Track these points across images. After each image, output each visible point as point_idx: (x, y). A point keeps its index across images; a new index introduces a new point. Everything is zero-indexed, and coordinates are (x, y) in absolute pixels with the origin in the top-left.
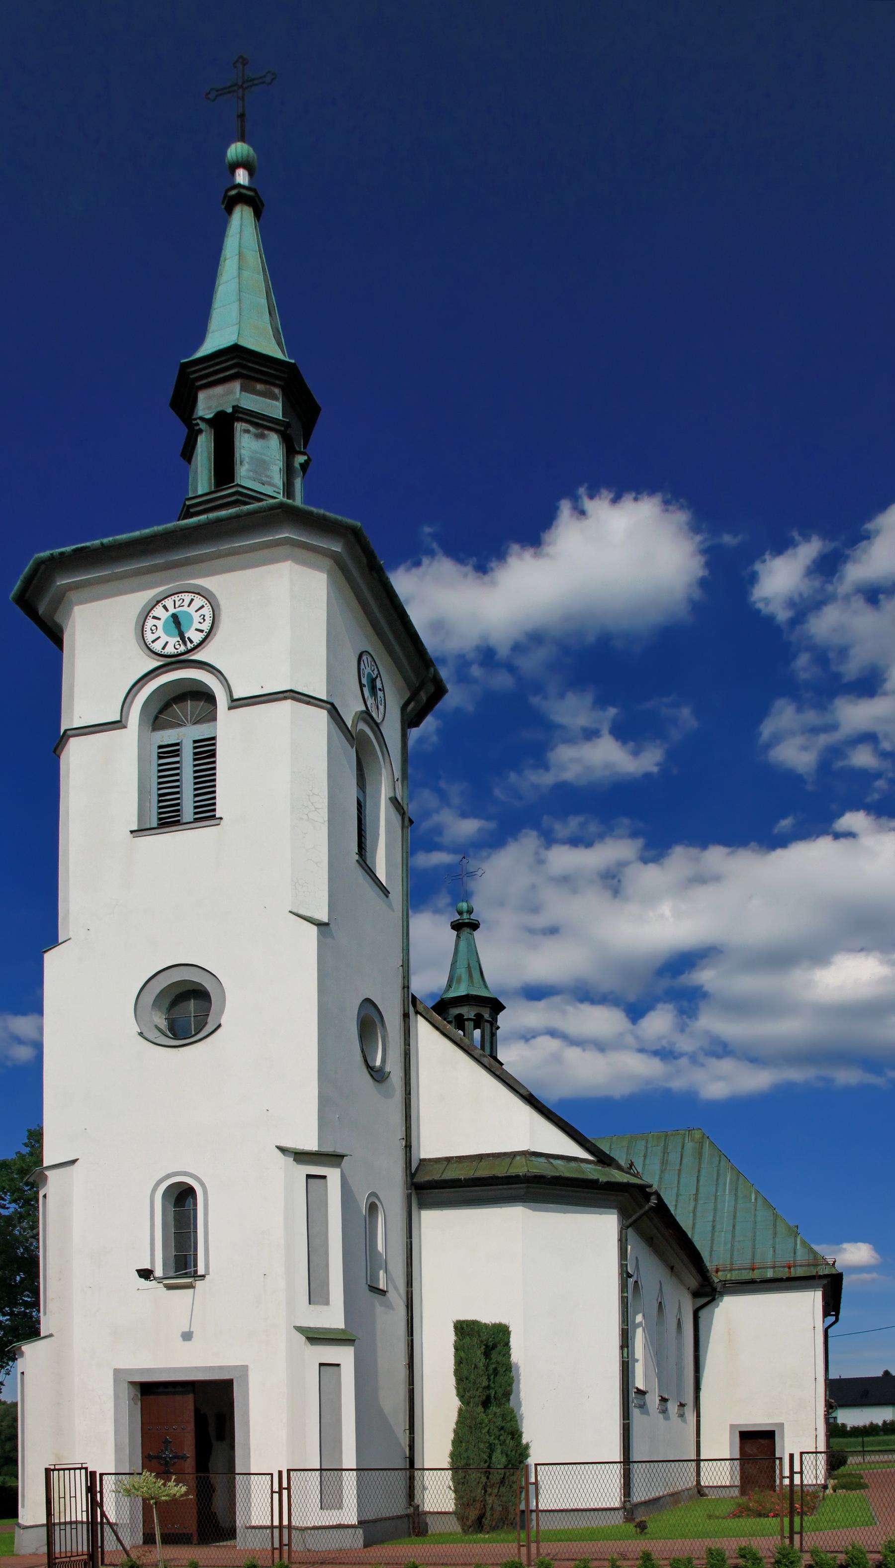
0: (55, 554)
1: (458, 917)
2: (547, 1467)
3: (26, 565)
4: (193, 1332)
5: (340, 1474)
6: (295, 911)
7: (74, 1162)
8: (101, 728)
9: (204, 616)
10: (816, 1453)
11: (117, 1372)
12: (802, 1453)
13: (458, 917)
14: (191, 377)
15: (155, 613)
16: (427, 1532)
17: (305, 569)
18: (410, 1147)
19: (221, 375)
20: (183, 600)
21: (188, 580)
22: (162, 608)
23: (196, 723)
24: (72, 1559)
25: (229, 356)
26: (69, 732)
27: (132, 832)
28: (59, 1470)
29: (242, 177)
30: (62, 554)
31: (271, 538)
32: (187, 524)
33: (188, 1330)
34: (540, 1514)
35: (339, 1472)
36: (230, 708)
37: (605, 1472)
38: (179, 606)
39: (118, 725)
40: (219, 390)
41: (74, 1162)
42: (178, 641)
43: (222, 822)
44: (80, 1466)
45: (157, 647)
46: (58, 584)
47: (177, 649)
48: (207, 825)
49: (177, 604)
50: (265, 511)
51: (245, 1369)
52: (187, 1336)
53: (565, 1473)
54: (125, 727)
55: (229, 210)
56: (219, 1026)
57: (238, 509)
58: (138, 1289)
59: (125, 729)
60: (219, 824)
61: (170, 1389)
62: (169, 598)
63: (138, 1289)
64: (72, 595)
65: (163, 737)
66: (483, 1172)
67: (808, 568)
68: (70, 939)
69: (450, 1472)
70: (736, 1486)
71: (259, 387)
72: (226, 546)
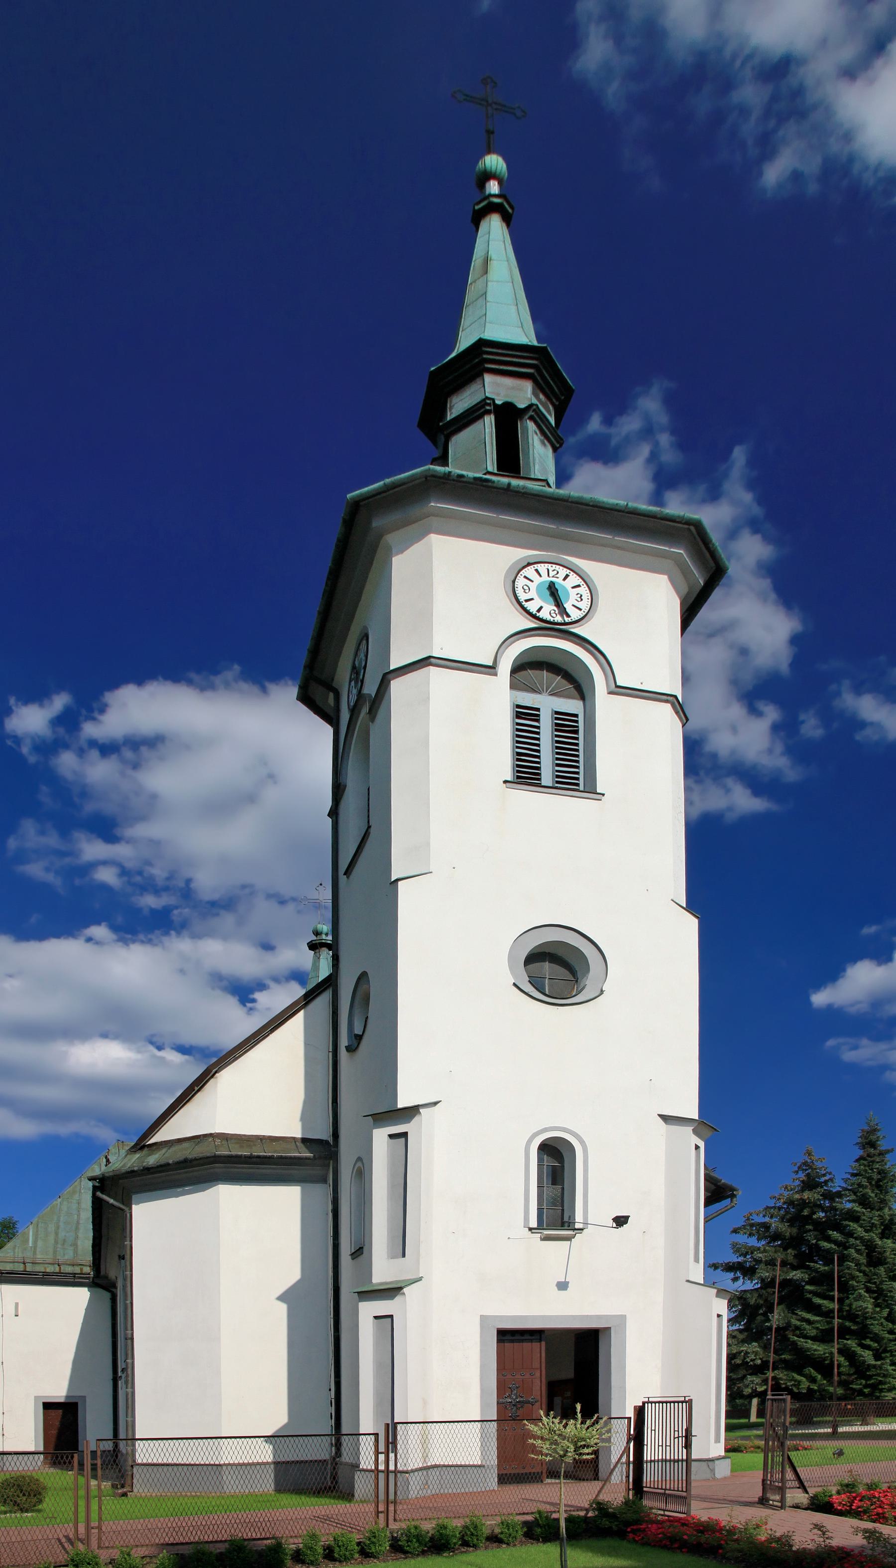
0: (453, 473)
1: (314, 938)
4: (568, 1282)
5: (356, 1440)
6: (675, 900)
7: (436, 1103)
8: (460, 665)
9: (581, 596)
11: (483, 1318)
13: (314, 938)
14: (485, 356)
16: (353, 1496)
17: (672, 588)
20: (558, 573)
21: (566, 556)
22: (534, 571)
23: (553, 694)
24: (667, 1492)
25: (531, 355)
26: (432, 660)
27: (505, 782)
28: (652, 1403)
29: (493, 187)
30: (462, 476)
33: (564, 1280)
34: (399, 1475)
35: (358, 1436)
36: (610, 693)
38: (553, 577)
39: (491, 669)
41: (436, 1103)
42: (554, 610)
43: (603, 798)
44: (683, 1399)
45: (532, 607)
47: (554, 617)
48: (574, 795)
49: (551, 574)
51: (623, 1318)
52: (563, 1286)
54: (496, 675)
55: (478, 218)
56: (602, 992)
58: (509, 1238)
59: (495, 677)
60: (601, 800)
61: (527, 1337)
62: (565, 569)
63: (509, 1238)
64: (434, 521)
65: (516, 697)
68: (431, 872)
70: (267, 1463)
71: (541, 396)
72: (621, 539)
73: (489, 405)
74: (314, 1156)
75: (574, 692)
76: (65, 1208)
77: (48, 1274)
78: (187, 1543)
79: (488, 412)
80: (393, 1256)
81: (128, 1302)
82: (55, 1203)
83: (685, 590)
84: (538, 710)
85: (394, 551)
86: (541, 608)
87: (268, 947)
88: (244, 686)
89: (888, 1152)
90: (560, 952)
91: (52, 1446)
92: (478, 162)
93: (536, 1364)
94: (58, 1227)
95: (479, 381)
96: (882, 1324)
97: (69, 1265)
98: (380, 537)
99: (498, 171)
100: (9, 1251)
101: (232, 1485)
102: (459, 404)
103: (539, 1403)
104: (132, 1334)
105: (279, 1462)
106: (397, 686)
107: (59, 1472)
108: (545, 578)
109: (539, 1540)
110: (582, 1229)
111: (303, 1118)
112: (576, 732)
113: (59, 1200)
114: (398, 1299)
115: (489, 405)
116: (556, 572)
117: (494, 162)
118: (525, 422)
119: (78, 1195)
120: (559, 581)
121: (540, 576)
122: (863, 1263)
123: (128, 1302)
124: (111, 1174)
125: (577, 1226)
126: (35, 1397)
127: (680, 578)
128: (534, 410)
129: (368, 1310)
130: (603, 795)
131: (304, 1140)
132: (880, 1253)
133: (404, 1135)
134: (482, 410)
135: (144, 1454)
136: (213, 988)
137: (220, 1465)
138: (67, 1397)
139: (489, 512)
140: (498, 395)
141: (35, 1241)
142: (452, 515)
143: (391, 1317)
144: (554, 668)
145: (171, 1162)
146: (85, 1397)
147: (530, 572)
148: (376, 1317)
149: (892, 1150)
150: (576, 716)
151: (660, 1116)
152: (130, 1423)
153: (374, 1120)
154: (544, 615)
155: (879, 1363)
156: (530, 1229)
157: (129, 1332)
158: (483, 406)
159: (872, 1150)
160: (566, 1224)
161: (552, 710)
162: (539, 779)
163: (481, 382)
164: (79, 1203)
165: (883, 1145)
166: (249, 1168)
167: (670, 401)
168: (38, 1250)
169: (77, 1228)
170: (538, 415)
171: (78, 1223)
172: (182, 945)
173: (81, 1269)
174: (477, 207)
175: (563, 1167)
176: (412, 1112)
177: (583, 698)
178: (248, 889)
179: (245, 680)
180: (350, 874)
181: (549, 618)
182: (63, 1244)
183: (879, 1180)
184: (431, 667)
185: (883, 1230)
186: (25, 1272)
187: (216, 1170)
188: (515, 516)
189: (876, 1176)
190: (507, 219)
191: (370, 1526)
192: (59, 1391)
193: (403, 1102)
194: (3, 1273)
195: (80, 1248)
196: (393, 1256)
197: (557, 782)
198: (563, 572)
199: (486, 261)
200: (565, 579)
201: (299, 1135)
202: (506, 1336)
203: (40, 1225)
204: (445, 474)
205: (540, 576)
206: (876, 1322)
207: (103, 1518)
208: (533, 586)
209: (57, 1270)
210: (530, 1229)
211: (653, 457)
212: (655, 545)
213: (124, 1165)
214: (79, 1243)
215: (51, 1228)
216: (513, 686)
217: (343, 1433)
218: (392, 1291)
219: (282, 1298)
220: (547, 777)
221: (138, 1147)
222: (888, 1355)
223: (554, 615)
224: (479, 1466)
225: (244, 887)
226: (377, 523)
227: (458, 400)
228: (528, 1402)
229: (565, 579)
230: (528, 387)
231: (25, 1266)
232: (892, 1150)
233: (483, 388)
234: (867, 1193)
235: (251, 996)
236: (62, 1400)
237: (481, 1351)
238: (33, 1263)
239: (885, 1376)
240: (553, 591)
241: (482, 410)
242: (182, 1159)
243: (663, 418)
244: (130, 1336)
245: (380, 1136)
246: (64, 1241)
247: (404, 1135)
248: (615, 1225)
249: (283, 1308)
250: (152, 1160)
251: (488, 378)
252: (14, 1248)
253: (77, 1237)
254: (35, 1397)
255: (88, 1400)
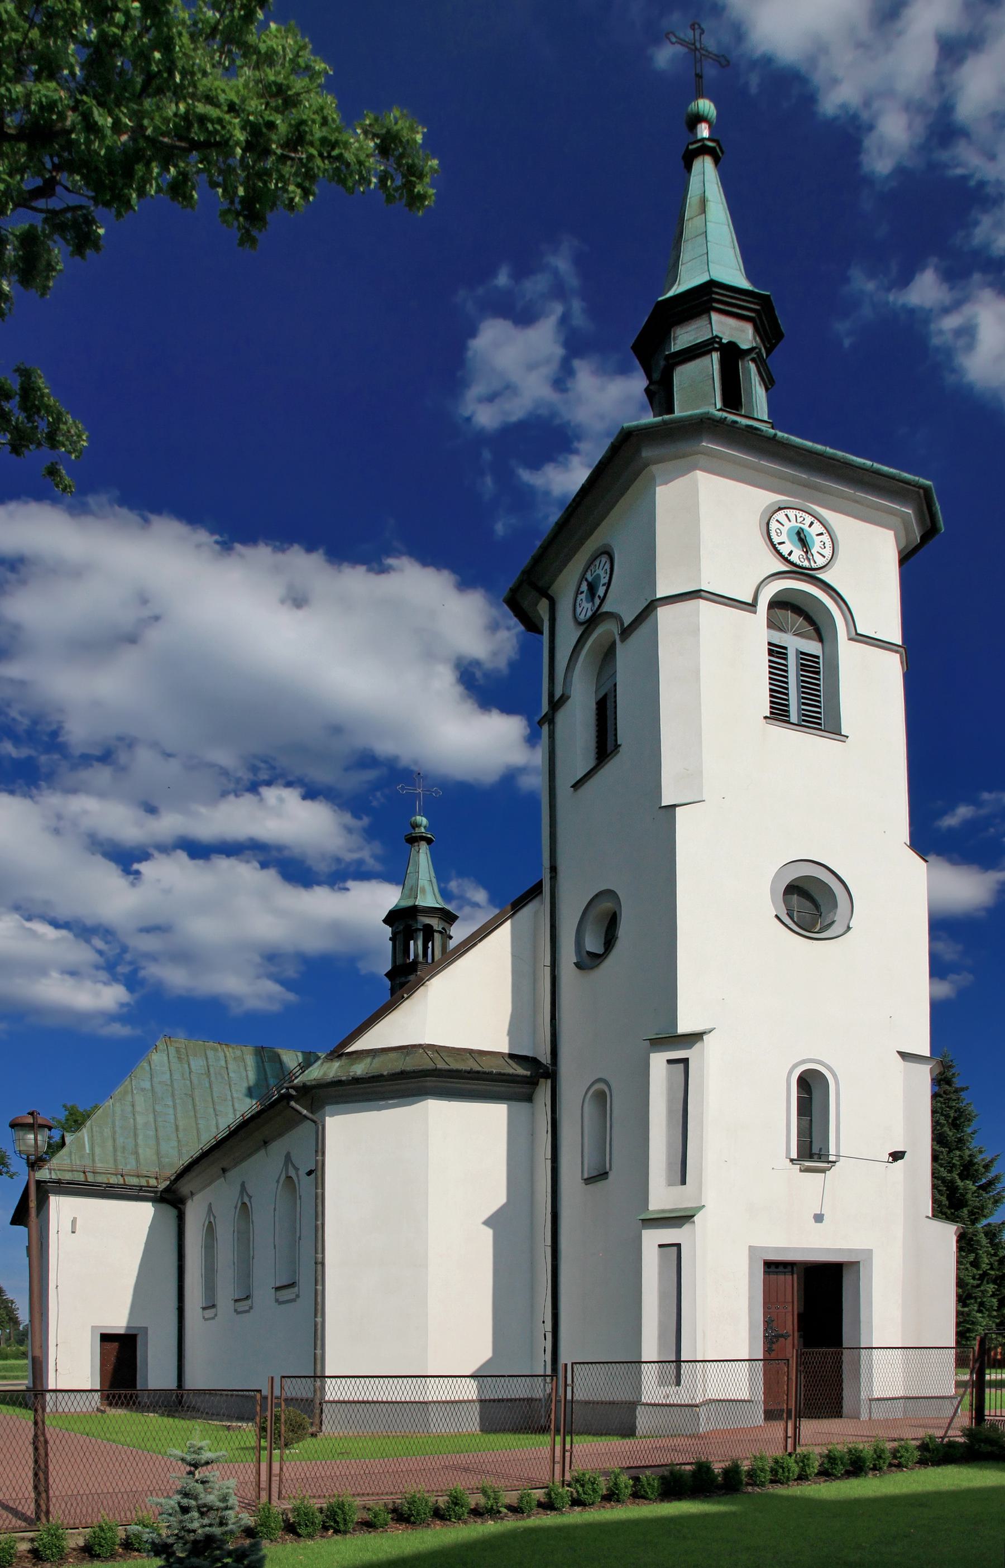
2: (358, 1380)
3: (814, 441)
8: (726, 601)
10: (315, 1377)
12: (572, 1364)
14: (714, 296)
15: (816, 524)
18: (339, 1044)
19: (740, 311)
26: (702, 593)
27: (766, 718)
29: (704, 131)
30: (736, 422)
31: (898, 507)
32: (853, 461)
36: (850, 639)
37: (341, 1388)
40: (732, 322)
43: (848, 740)
45: (784, 550)
46: (704, 444)
50: (914, 486)
53: (417, 1387)
54: (755, 613)
55: (689, 159)
56: (849, 928)
57: (898, 472)
64: (702, 460)
66: (470, 1065)
67: (370, 570)
69: (761, 1363)
70: (473, 1401)
71: (758, 339)
73: (717, 343)
74: (531, 1074)
75: (813, 634)
76: (118, 1109)
77: (112, 1186)
78: (662, 1465)
79: (716, 350)
80: (670, 1184)
81: (319, 1223)
82: (107, 1104)
83: (903, 545)
84: (785, 648)
85: (658, 481)
86: (791, 552)
87: (152, 810)
88: (124, 511)
89: (963, 1089)
90: (806, 886)
91: (107, 1384)
92: (690, 103)
93: (789, 1298)
94: (114, 1133)
95: (705, 317)
96: (967, 1269)
97: (133, 1176)
98: (646, 465)
99: (709, 117)
100: (65, 1158)
101: (439, 1424)
102: (684, 337)
103: (791, 1338)
104: (323, 1258)
105: (486, 1401)
106: (663, 613)
107: (128, 1413)
108: (793, 523)
109: (928, 1464)
110: (835, 1162)
111: (511, 1033)
112: (818, 673)
113: (111, 1101)
114: (687, 1227)
115: (717, 343)
116: (802, 519)
117: (706, 106)
118: (746, 362)
119: (130, 1096)
120: (806, 527)
121: (790, 521)
122: (945, 1205)
123: (319, 1223)
124: (313, 1083)
125: (832, 1158)
126: (92, 1327)
127: (902, 533)
128: (757, 353)
129: (652, 1239)
130: (847, 737)
131: (512, 1056)
132: (962, 1195)
133: (685, 1061)
134: (711, 347)
135: (333, 1391)
136: (93, 854)
137: (426, 1403)
138: (128, 1328)
139: (738, 452)
140: (724, 333)
141: (92, 1148)
142: (734, 461)
143: (678, 1246)
144: (798, 610)
145: (385, 1073)
146: (146, 1328)
147: (780, 515)
148: (660, 1246)
149: (967, 1088)
150: (818, 657)
151: (899, 1052)
152: (319, 1357)
153: (651, 1044)
154: (794, 558)
155: (966, 1309)
156: (792, 1160)
157: (320, 1256)
158: (712, 344)
159: (947, 1087)
160: (816, 1157)
161: (797, 650)
162: (788, 716)
163: (707, 318)
164: (133, 1106)
165: (957, 1083)
166: (495, 1086)
167: (579, 261)
168: (97, 1158)
169: (136, 1135)
170: (760, 360)
171: (135, 1128)
172: (53, 800)
173: (148, 1182)
174: (691, 147)
175: (811, 1098)
176: (695, 1038)
177: (821, 640)
178: (130, 743)
179: (121, 505)
180: (578, 788)
181: (799, 563)
182: (123, 1152)
183: (955, 1119)
184: (701, 600)
185: (961, 1170)
186: (86, 1183)
187: (428, 1084)
188: (780, 465)
189: (952, 1114)
190: (717, 161)
191: (779, 1453)
192: (118, 1322)
193: (684, 1027)
194: (63, 1183)
195: (141, 1157)
196: (670, 1184)
197: (804, 721)
198: (809, 519)
199: (703, 202)
200: (810, 526)
201: (505, 1049)
202: (772, 1267)
203: (94, 1129)
204: (721, 418)
205: (790, 521)
206: (963, 1267)
207: (285, 1458)
208: (784, 530)
209: (121, 1181)
210: (792, 1160)
211: (564, 320)
212: (888, 501)
213: (325, 1074)
214: (140, 1151)
215: (107, 1132)
216: (771, 625)
217: (173, 1385)
218: (682, 1219)
219: (487, 1223)
220: (794, 718)
221: (336, 1054)
222: (972, 1301)
223: (802, 560)
224: (749, 1401)
225: (120, 739)
226: (646, 453)
227: (683, 331)
228: (782, 1336)
229: (810, 526)
230: (749, 329)
231: (86, 1176)
232: (967, 1088)
233: (709, 326)
234: (945, 1131)
235: (136, 866)
236: (122, 1331)
237: (750, 1282)
238: (93, 1173)
239: (973, 1323)
240: (802, 539)
241: (711, 347)
242: (398, 1070)
243: (573, 281)
244: (320, 1260)
245: (658, 1061)
246: (124, 1148)
247: (685, 1061)
248: (891, 1159)
249: (488, 1233)
250: (359, 1069)
251: (715, 316)
252: (71, 1153)
253: (136, 1145)
254: (92, 1327)
255: (150, 1332)
